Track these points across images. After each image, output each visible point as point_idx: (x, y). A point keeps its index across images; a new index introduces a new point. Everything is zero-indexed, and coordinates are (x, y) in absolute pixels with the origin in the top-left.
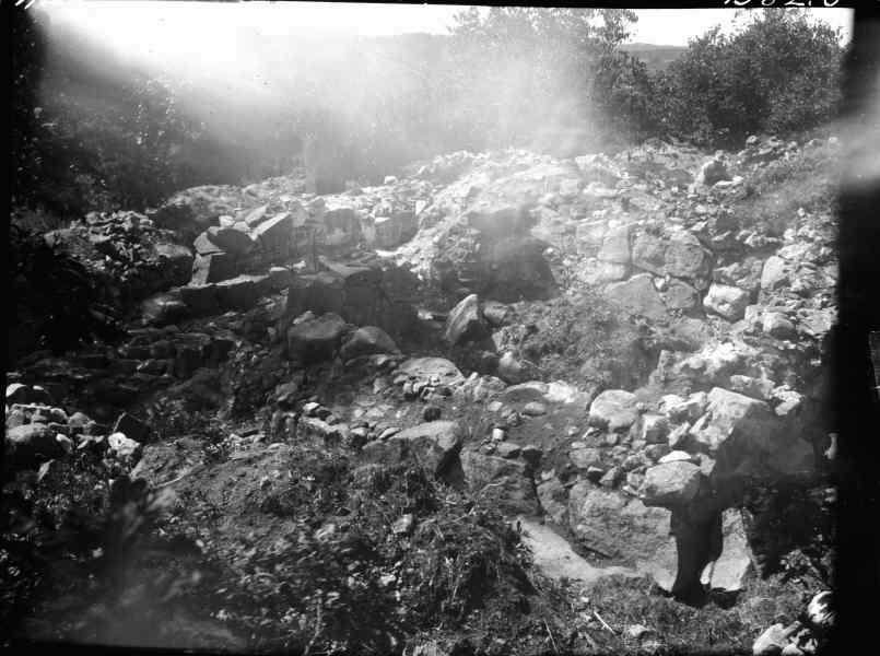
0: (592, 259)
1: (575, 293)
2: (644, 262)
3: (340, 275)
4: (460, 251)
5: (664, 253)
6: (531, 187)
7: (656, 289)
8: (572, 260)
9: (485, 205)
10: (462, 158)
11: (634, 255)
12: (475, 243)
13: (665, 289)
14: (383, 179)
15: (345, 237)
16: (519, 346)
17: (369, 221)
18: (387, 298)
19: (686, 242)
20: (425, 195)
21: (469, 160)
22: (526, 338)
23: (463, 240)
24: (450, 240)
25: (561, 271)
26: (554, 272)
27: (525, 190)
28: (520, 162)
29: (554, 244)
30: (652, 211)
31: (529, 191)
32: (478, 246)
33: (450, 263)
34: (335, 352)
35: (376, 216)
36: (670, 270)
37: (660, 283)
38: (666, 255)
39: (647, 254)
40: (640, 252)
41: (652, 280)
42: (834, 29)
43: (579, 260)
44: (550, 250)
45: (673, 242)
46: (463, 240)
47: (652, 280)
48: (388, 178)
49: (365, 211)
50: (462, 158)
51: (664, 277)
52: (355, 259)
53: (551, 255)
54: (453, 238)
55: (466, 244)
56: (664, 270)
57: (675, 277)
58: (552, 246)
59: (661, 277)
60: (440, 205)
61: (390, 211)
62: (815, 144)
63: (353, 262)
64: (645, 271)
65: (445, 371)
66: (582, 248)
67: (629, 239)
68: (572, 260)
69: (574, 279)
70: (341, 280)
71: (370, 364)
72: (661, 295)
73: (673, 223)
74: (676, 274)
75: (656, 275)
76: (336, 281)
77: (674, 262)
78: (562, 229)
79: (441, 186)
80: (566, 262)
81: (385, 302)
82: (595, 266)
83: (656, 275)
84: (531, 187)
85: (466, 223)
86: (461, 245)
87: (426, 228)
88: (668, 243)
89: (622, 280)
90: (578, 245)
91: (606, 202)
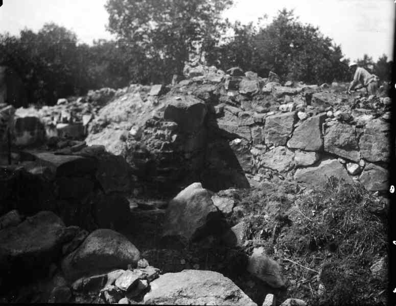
0: (282, 148)
1: (261, 178)
2: (338, 149)
3: (51, 164)
4: (157, 142)
5: (358, 140)
6: (213, 87)
7: (349, 173)
8: (261, 149)
9: (180, 99)
10: (107, 92)
11: (326, 144)
12: (172, 134)
13: (358, 173)
14: (57, 101)
15: (32, 139)
16: (271, 240)
17: (52, 127)
18: (102, 189)
19: (383, 130)
20: (89, 112)
21: (112, 94)
22: (278, 231)
23: (159, 132)
24: (146, 134)
25: (249, 159)
26: (241, 160)
27: (209, 89)
28: (192, 71)
29: (241, 135)
30: (336, 104)
31: (212, 91)
32: (174, 137)
33: (147, 154)
34: (53, 267)
35: (57, 123)
36: (365, 156)
37: (352, 168)
38: (361, 142)
39: (341, 141)
40: (334, 140)
41: (345, 165)
42: (315, 28)
43: (268, 149)
44: (237, 141)
45: (368, 129)
46: (159, 132)
47: (345, 165)
48: (60, 101)
49: (48, 118)
50: (107, 92)
51: (358, 163)
52: (62, 147)
53: (239, 145)
54: (149, 131)
55: (163, 136)
56: (356, 155)
57: (370, 162)
58: (240, 138)
59: (353, 162)
60: (105, 116)
61: (69, 119)
62: (325, 86)
63: (59, 151)
64: (336, 157)
65: (223, 292)
66: (270, 139)
67: (321, 129)
68: (261, 149)
69: (261, 166)
70: (53, 170)
71: (109, 287)
72: (354, 178)
73: (361, 113)
74: (372, 159)
75: (348, 161)
76: (47, 171)
77: (370, 147)
78: (250, 121)
79: (98, 107)
80: (254, 151)
81: (100, 193)
82: (284, 154)
83: (348, 161)
84: (213, 87)
85: (162, 116)
86: (157, 137)
87: (94, 133)
88: (361, 130)
89: (313, 165)
90: (268, 136)
91: (287, 98)
